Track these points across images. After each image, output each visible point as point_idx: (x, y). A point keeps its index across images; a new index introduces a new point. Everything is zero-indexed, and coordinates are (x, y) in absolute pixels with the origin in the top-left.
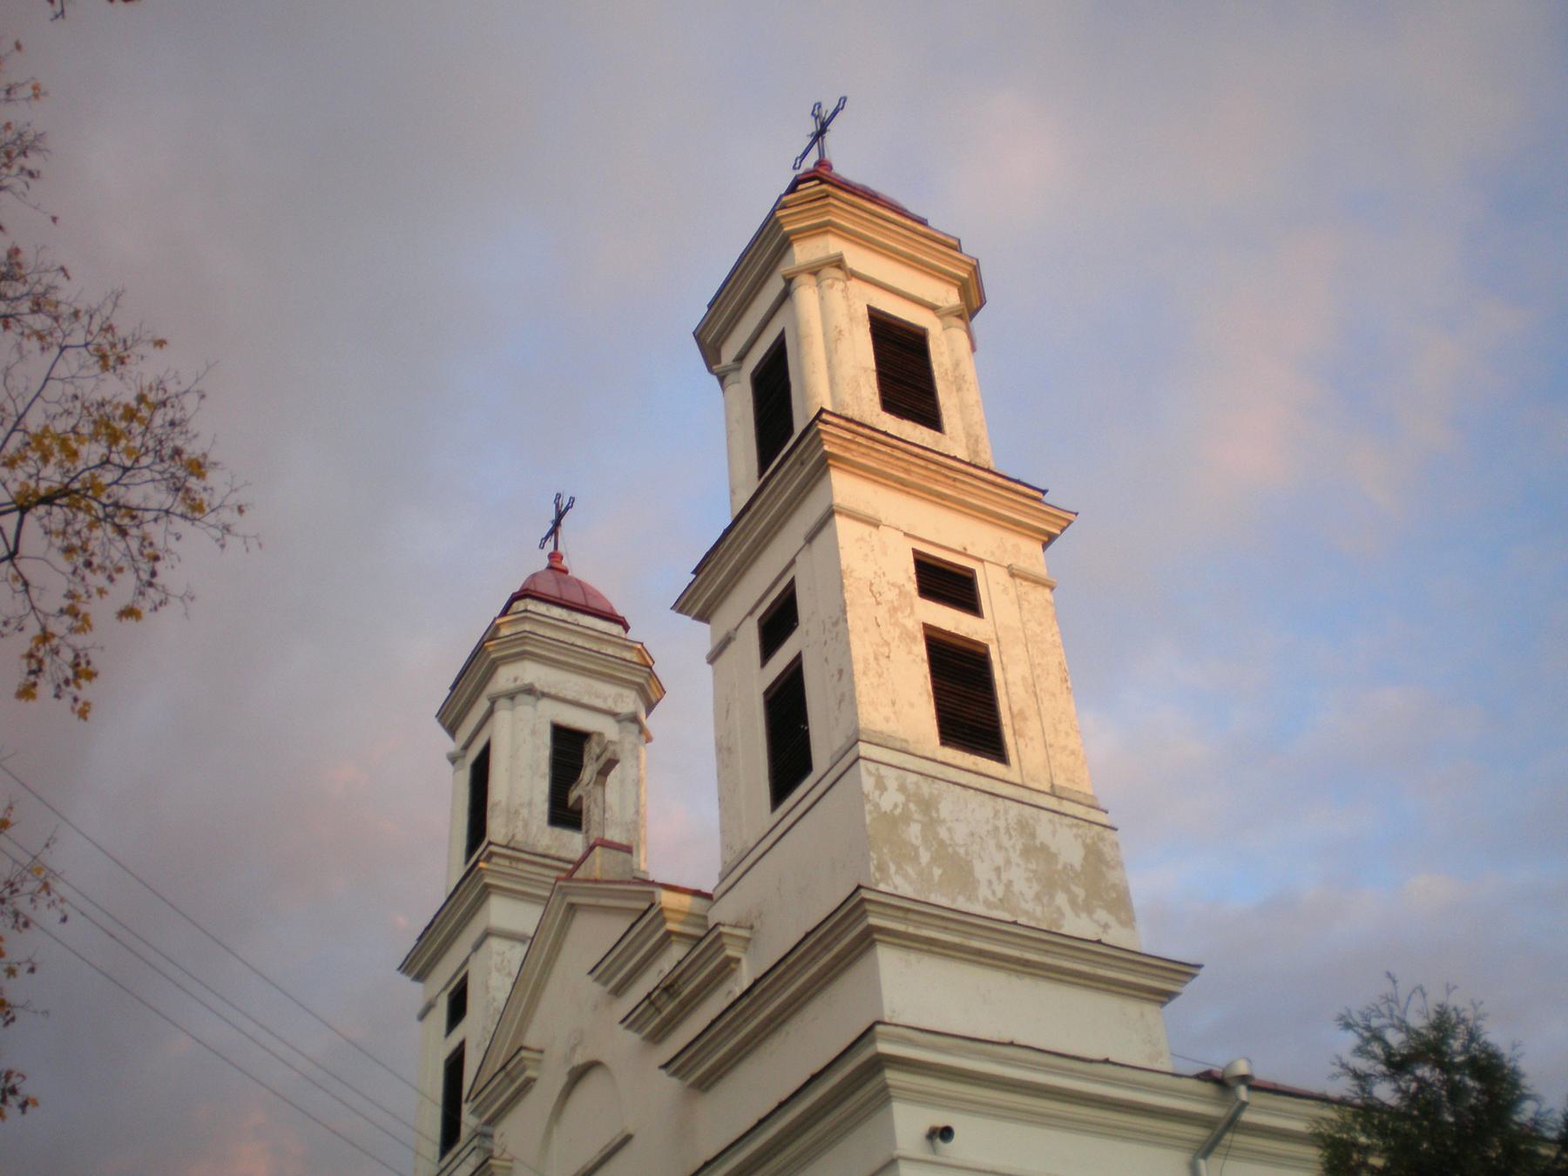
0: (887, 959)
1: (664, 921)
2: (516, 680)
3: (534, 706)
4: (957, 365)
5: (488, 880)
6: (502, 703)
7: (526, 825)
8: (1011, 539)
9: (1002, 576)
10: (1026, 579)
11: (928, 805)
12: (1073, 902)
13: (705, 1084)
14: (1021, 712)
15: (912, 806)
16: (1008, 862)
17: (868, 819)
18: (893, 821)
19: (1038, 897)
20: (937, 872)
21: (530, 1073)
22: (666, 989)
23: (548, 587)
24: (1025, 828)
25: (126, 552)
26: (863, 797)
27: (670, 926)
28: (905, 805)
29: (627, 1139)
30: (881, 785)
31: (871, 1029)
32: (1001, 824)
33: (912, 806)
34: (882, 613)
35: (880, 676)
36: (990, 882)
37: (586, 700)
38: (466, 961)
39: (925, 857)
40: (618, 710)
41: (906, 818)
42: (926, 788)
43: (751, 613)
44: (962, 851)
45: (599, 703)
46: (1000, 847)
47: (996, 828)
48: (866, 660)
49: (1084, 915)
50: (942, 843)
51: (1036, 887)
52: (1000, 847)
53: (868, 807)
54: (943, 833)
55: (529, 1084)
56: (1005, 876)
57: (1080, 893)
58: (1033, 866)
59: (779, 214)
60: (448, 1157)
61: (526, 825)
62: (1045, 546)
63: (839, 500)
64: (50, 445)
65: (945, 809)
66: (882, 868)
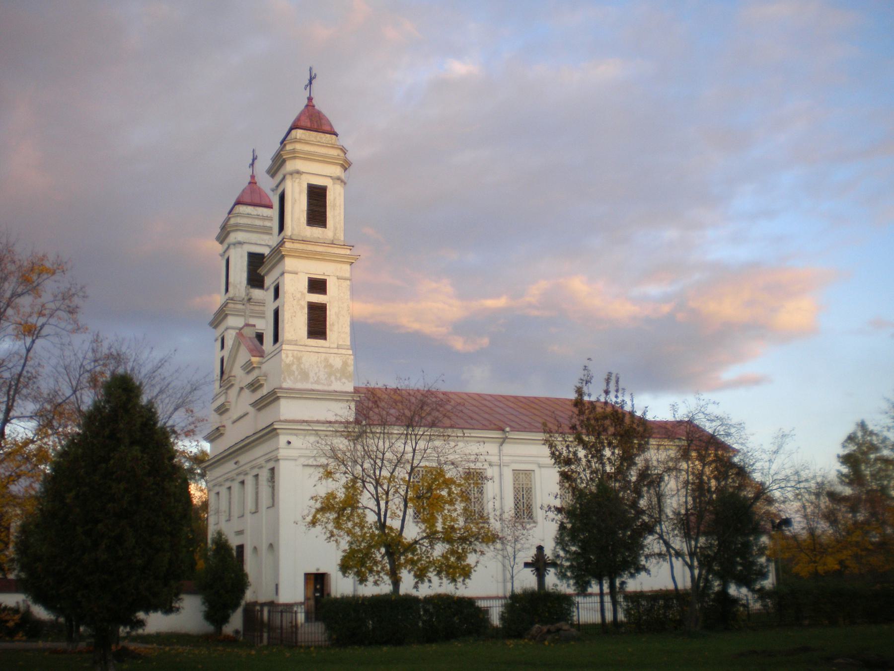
0: (283, 402)
1: (252, 364)
2: (235, 238)
3: (242, 248)
4: (335, 199)
5: (227, 312)
6: (232, 246)
7: (239, 290)
8: (339, 266)
9: (335, 279)
10: (341, 279)
11: (299, 359)
12: (336, 379)
13: (259, 410)
14: (333, 323)
15: (295, 360)
16: (319, 371)
17: (282, 366)
18: (289, 366)
19: (326, 379)
20: (299, 377)
21: (233, 382)
22: (252, 384)
23: (247, 199)
24: (326, 360)
25: (84, 352)
26: (281, 360)
27: (255, 365)
28: (293, 361)
29: (247, 413)
30: (287, 356)
31: (272, 423)
32: (319, 360)
33: (295, 360)
34: (295, 302)
35: (292, 322)
36: (313, 377)
37: (259, 242)
38: (223, 332)
39: (296, 373)
40: (269, 244)
41: (293, 364)
42: (299, 354)
43: (273, 283)
44: (307, 370)
45: (263, 243)
46: (318, 367)
47: (317, 362)
48: (288, 319)
49: (338, 381)
50: (301, 369)
51: (326, 376)
52: (318, 367)
53: (283, 363)
54: (302, 366)
55: (232, 385)
56: (317, 375)
57: (338, 375)
58: (326, 370)
59: (281, 153)
60: (277, 282)
61: (239, 290)
62: (351, 265)
63: (286, 268)
64: (52, 452)
65: (304, 360)
66: (284, 379)
